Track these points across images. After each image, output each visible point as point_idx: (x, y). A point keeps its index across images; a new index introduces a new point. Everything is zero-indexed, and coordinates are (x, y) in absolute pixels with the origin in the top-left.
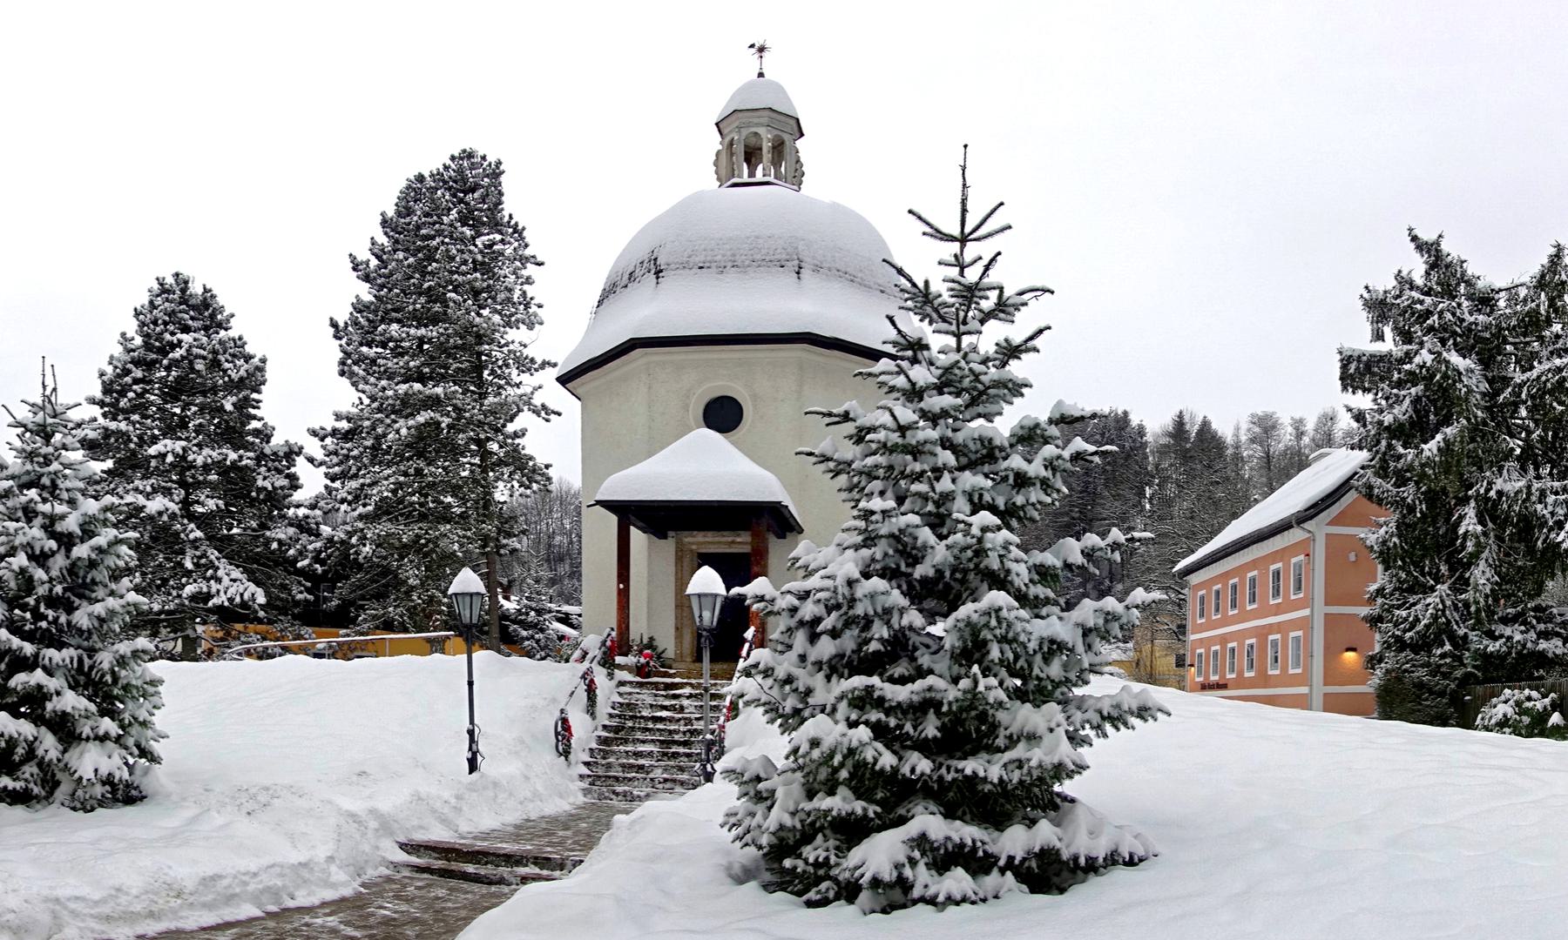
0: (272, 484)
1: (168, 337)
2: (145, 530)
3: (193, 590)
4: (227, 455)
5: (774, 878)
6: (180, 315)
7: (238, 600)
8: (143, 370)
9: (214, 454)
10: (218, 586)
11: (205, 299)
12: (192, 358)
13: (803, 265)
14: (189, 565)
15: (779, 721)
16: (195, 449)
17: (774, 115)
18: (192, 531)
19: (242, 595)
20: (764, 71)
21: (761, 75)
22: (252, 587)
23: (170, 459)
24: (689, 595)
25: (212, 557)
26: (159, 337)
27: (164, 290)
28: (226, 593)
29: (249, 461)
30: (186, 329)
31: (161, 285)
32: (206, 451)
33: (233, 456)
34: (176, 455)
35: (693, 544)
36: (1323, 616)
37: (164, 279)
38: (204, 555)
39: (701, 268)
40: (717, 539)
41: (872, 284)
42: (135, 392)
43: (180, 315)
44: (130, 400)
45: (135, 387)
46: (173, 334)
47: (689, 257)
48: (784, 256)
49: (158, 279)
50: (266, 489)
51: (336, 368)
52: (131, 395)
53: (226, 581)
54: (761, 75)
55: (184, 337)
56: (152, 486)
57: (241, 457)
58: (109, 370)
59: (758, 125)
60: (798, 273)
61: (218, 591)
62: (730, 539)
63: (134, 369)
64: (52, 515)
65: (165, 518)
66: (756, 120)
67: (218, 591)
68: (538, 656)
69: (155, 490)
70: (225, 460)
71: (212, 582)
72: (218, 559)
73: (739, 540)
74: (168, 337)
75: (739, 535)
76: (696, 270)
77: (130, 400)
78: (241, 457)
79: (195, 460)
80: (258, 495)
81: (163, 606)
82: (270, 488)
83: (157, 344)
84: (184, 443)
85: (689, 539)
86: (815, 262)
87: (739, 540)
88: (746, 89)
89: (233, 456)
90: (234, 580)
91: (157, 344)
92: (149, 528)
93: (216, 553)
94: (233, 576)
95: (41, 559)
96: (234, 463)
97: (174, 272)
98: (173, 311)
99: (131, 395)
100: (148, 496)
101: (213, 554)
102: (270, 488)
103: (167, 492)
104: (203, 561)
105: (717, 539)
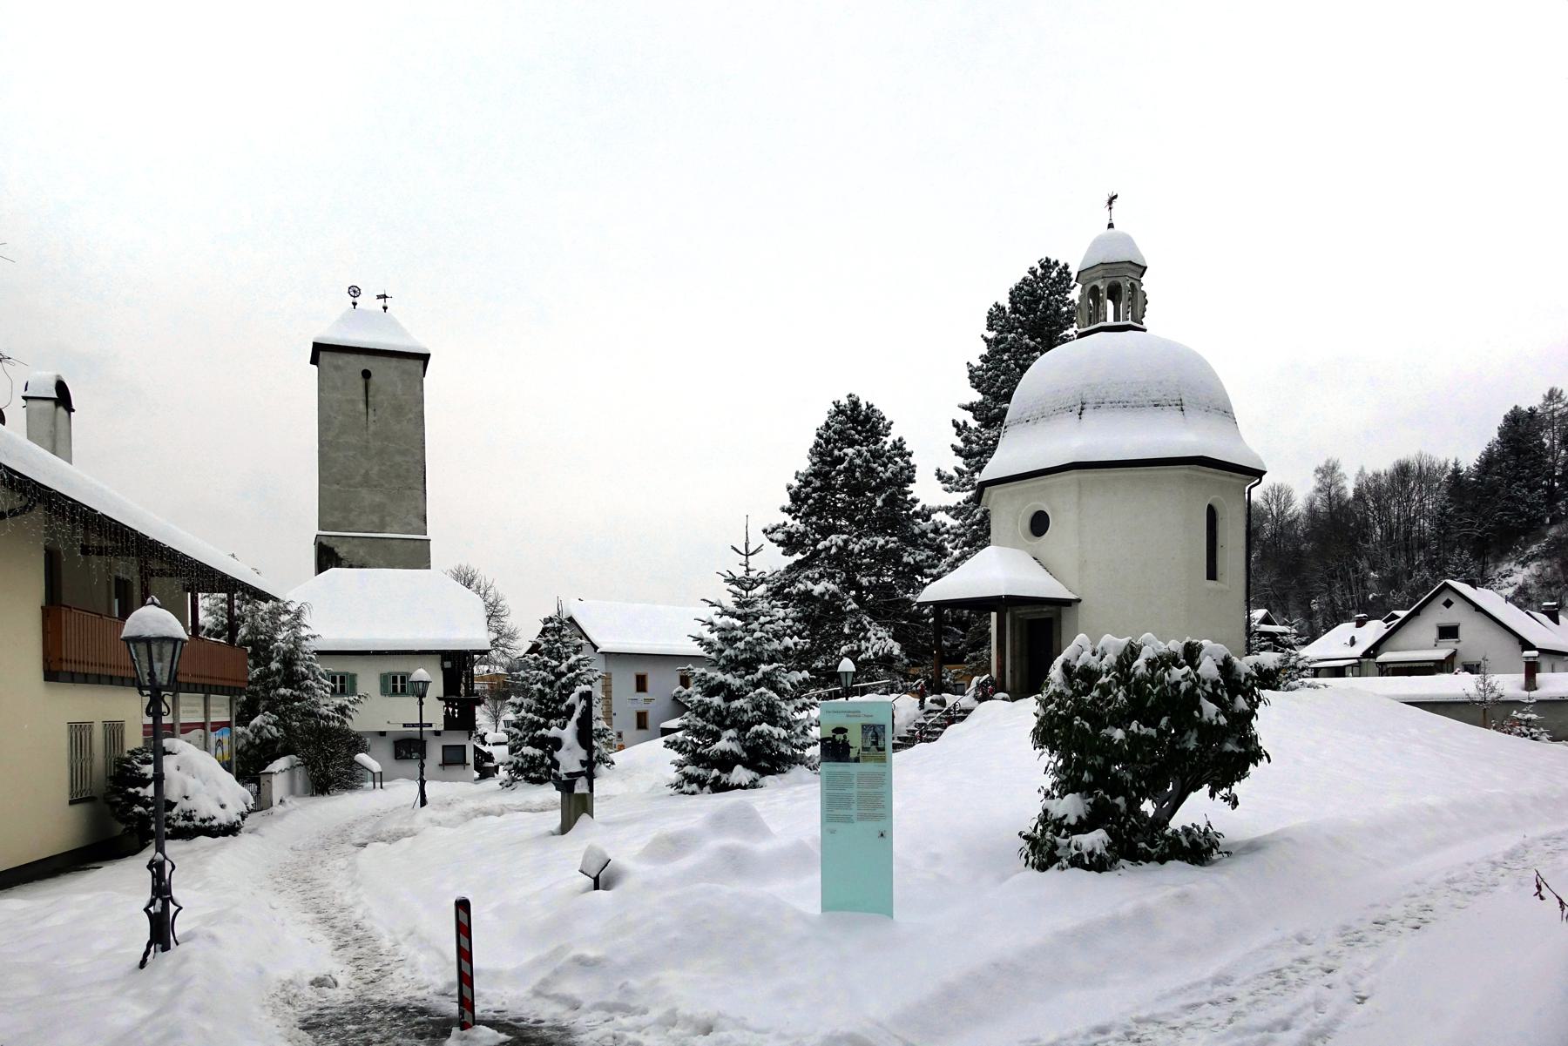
0: (914, 560)
1: (836, 452)
2: (815, 607)
3: (847, 649)
4: (876, 542)
5: (1065, 822)
6: (848, 432)
7: (881, 653)
8: (821, 480)
9: (868, 542)
10: (867, 645)
11: (867, 414)
12: (853, 468)
13: (1085, 406)
14: (846, 630)
15: (725, 713)
16: (855, 539)
17: (1105, 267)
18: (850, 604)
19: (883, 649)
20: (1114, 222)
21: (1111, 226)
22: (891, 642)
23: (834, 550)
24: (839, 673)
25: (865, 622)
26: (831, 453)
27: (839, 411)
28: (872, 648)
29: (892, 544)
30: (851, 444)
31: (837, 407)
32: (864, 540)
33: (881, 541)
34: (839, 547)
35: (1020, 614)
36: (66, 728)
37: (839, 402)
38: (859, 622)
39: (1028, 421)
41: (1145, 403)
42: (814, 498)
43: (848, 432)
44: (809, 506)
45: (813, 495)
46: (840, 450)
47: (1022, 414)
48: (1073, 403)
49: (834, 403)
50: (910, 563)
51: (917, 469)
52: (811, 501)
53: (873, 639)
54: (1111, 226)
55: (850, 451)
56: (820, 573)
57: (887, 542)
58: (796, 484)
59: (1096, 279)
60: (1080, 414)
61: (867, 649)
62: (1039, 610)
63: (814, 480)
64: (306, 764)
65: (827, 597)
66: (1094, 275)
67: (867, 649)
68: (880, 691)
69: (822, 576)
70: (876, 545)
71: (863, 642)
72: (870, 623)
74: (836, 452)
76: (1025, 423)
77: (809, 506)
78: (887, 542)
79: (853, 549)
80: (904, 569)
81: (827, 663)
82: (912, 563)
83: (829, 459)
84: (845, 537)
85: (1018, 612)
86: (1098, 400)
87: (1045, 610)
88: (1097, 244)
89: (881, 541)
90: (879, 639)
91: (829, 459)
92: (818, 605)
93: (868, 619)
94: (879, 636)
95: (551, 684)
96: (882, 547)
97: (848, 394)
98: (841, 429)
99: (811, 501)
100: (816, 582)
101: (866, 619)
102: (912, 563)
103: (832, 577)
104: (858, 626)
105: (1034, 610)
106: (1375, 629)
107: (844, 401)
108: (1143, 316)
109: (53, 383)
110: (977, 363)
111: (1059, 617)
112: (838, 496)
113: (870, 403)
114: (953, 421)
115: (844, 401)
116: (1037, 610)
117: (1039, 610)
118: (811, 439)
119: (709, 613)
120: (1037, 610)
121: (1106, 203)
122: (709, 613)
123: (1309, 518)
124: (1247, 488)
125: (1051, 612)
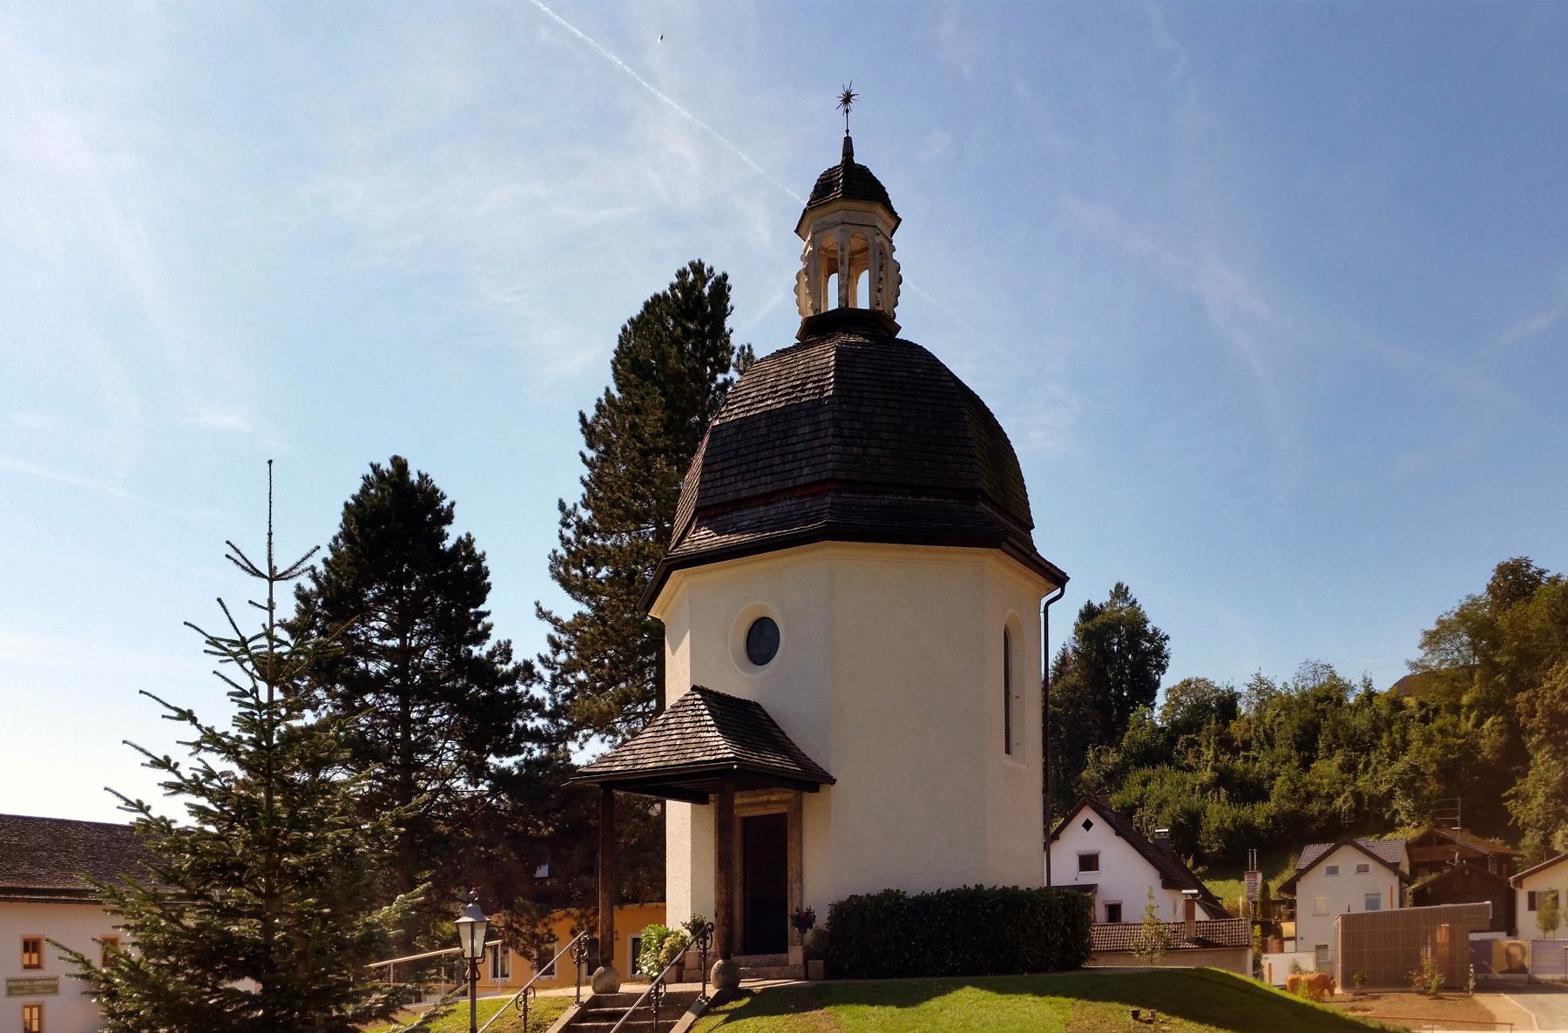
40: (754, 799)
62: (765, 798)
73: (774, 798)
75: (772, 793)
87: (774, 798)
105: (754, 799)
106: (258, 675)
107: (386, 466)
108: (896, 304)
109: (833, 774)
110: (590, 414)
111: (799, 810)
112: (371, 624)
113: (423, 473)
114: (560, 501)
115: (386, 466)
116: (761, 799)
117: (765, 798)
118: (648, 297)
119: (173, 740)
120: (761, 799)
121: (839, 102)
122: (173, 740)
123: (1084, 640)
124: (1044, 601)
125: (784, 802)
